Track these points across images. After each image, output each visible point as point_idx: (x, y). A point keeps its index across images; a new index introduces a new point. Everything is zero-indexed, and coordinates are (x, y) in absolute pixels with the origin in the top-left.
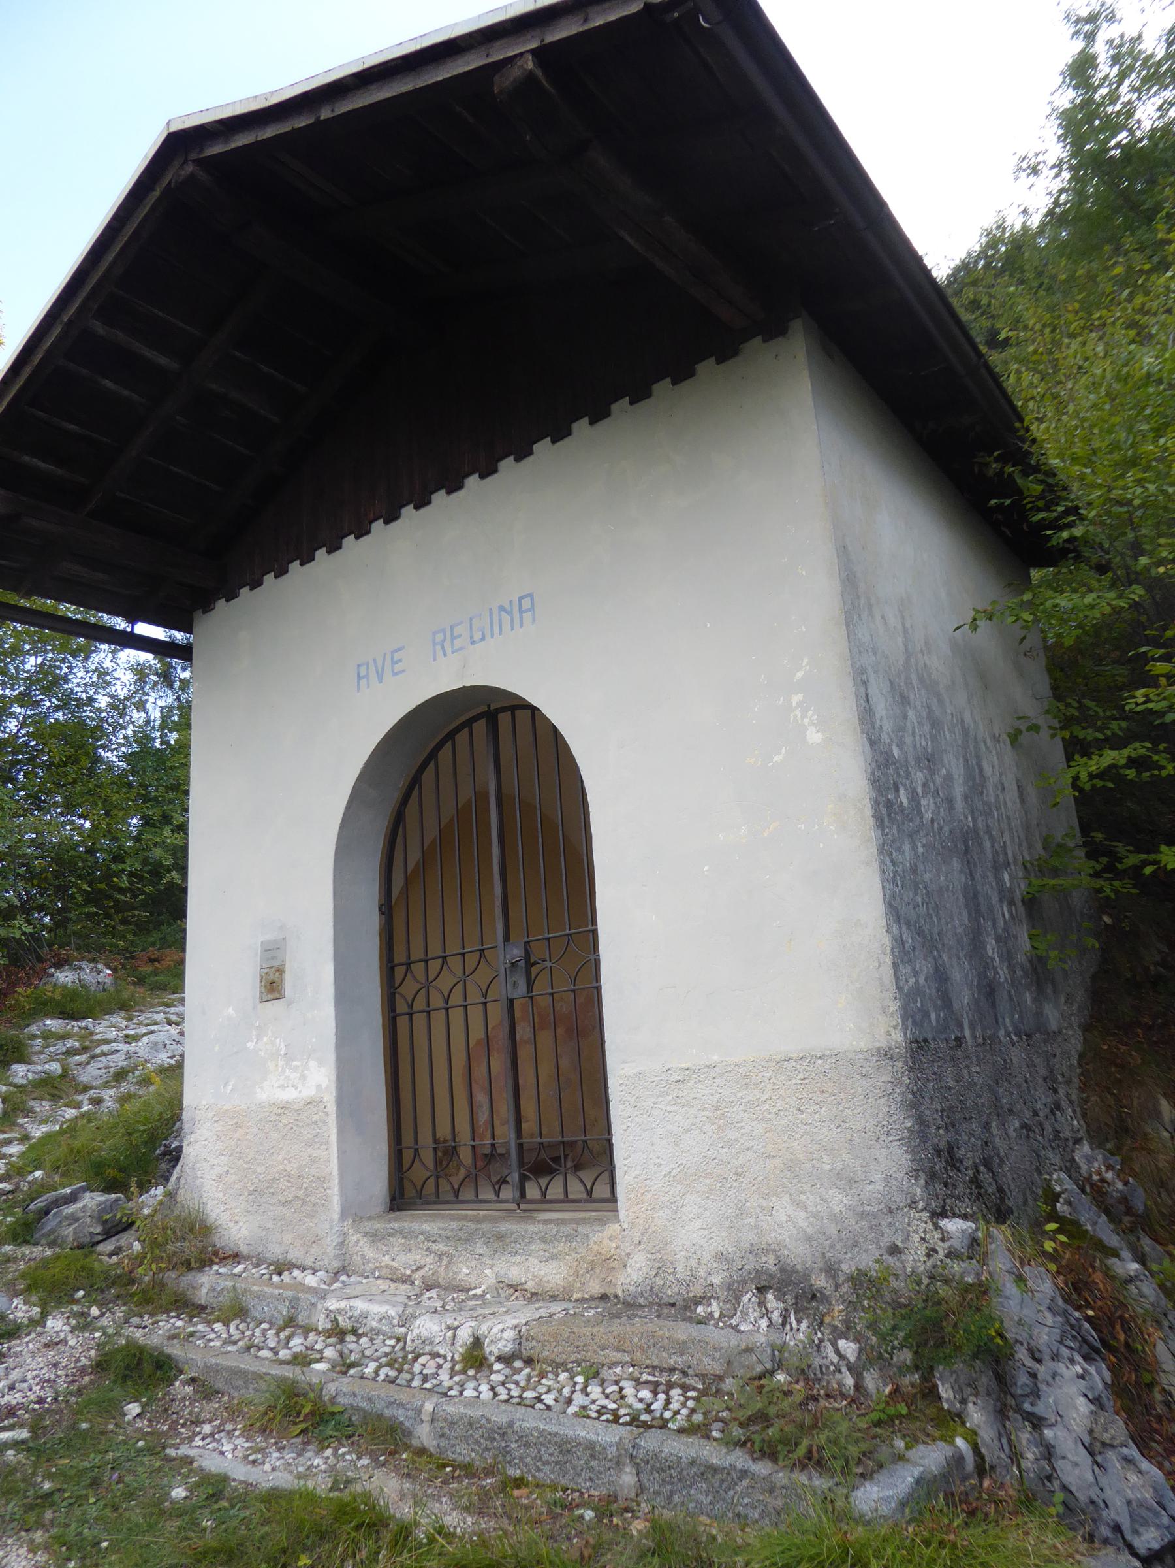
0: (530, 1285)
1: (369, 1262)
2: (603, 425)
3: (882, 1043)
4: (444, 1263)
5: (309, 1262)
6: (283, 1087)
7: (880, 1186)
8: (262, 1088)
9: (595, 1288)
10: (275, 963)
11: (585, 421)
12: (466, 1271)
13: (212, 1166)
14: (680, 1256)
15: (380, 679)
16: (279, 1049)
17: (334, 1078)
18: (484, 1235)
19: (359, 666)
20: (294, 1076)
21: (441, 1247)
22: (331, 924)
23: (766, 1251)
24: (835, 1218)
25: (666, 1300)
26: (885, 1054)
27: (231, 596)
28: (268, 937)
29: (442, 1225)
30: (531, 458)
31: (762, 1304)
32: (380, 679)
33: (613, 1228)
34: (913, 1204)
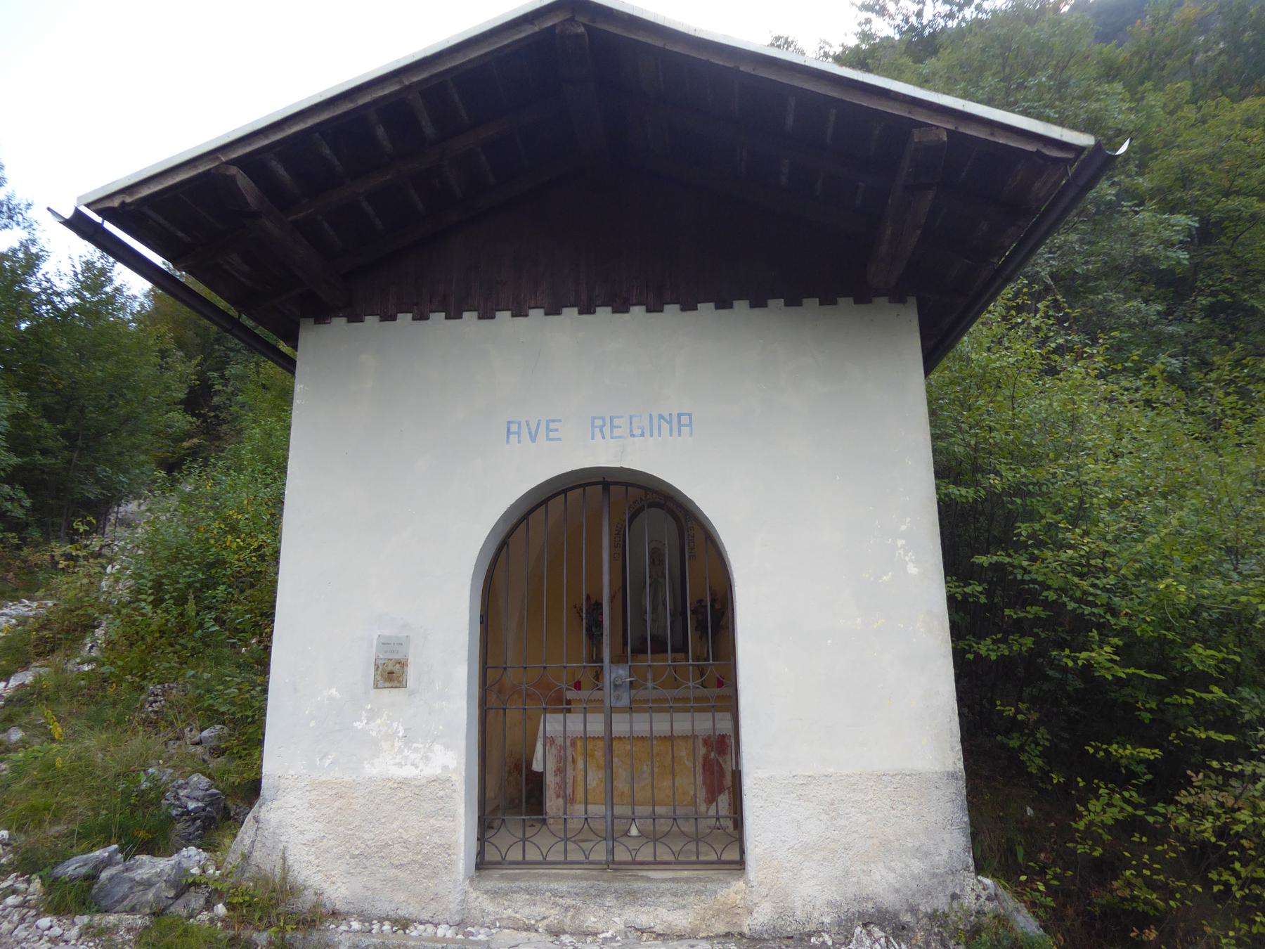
0: (658, 929)
1: (488, 914)
2: (757, 311)
3: (950, 768)
4: (570, 914)
5: (425, 916)
6: (400, 765)
7: (945, 857)
8: (373, 765)
9: (721, 928)
10: (396, 657)
11: (575, 310)
12: (593, 919)
13: (302, 832)
14: (799, 904)
15: (533, 439)
16: (397, 732)
17: (463, 761)
18: (616, 891)
19: (509, 422)
20: (414, 756)
21: (569, 901)
22: (467, 632)
23: (867, 899)
24: (914, 878)
25: (785, 934)
26: (952, 776)
27: (355, 317)
28: (387, 632)
29: (571, 884)
30: (798, 308)
31: (869, 934)
32: (533, 439)
33: (740, 884)
34: (966, 868)
